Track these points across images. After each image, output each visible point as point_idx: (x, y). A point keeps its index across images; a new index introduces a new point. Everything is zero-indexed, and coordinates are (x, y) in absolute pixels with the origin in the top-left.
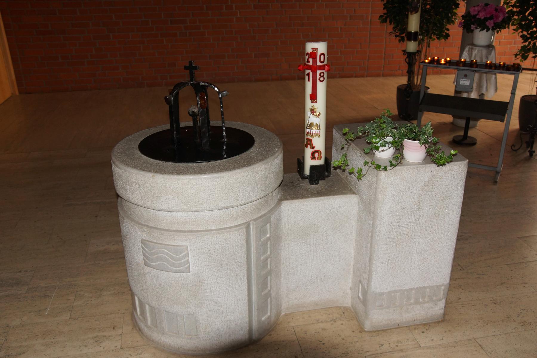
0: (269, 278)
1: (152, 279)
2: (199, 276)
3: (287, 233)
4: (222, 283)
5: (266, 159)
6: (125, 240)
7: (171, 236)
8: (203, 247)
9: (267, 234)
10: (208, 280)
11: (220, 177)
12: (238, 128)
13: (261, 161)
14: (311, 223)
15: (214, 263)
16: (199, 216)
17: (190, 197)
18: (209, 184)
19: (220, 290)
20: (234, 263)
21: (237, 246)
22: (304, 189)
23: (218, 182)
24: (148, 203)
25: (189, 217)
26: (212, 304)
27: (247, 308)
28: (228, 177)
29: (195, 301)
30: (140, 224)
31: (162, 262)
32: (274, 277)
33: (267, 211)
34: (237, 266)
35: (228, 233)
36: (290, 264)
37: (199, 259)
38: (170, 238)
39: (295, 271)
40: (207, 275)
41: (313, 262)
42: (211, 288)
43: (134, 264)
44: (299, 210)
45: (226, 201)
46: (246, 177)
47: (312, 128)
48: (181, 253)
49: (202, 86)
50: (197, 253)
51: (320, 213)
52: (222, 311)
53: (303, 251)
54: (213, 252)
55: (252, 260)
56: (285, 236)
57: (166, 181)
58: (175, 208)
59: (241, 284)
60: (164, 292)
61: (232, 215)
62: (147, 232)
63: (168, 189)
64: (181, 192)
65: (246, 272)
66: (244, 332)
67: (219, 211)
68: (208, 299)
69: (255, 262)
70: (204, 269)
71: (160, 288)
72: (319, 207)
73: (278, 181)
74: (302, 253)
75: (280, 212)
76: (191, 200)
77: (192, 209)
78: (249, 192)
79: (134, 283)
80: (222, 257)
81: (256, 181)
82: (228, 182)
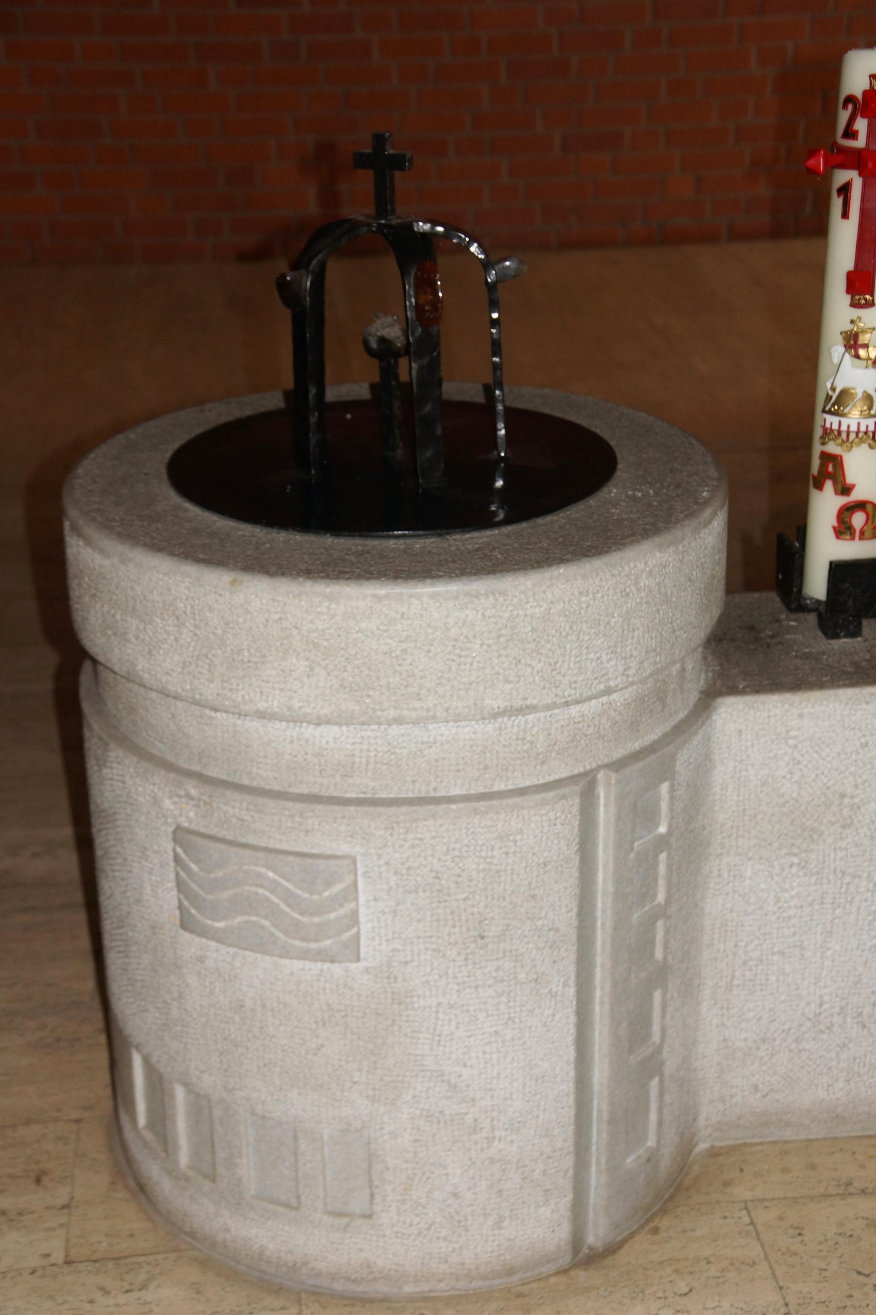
0: (657, 995)
1: (207, 984)
2: (392, 976)
3: (730, 824)
4: (480, 1010)
5: (666, 528)
6: (103, 833)
7: (291, 816)
8: (416, 864)
9: (657, 825)
10: (428, 993)
11: (493, 594)
12: (547, 410)
13: (647, 534)
14: (828, 788)
15: (454, 926)
16: (403, 741)
17: (373, 668)
18: (448, 620)
19: (470, 1037)
20: (530, 931)
21: (545, 865)
22: (799, 654)
23: (486, 614)
24: (211, 685)
25: (365, 747)
26: (437, 1089)
27: (569, 1114)
28: (524, 592)
29: (370, 1076)
30: (170, 767)
31: (254, 918)
32: (676, 995)
33: (660, 734)
34: (543, 945)
35: (512, 811)
36: (736, 946)
37: (395, 911)
38: (289, 824)
39: (756, 975)
40: (424, 976)
41: (829, 945)
42: (439, 1027)
43: (139, 925)
44: (784, 735)
45: (512, 685)
46: (591, 596)
47: (846, 411)
48: (329, 884)
49: (424, 234)
50: (390, 888)
51: (866, 749)
52: (475, 1120)
53: (792, 898)
54: (453, 886)
55: (599, 923)
56: (724, 835)
57: (285, 605)
58: (314, 708)
59: (553, 1015)
60: (254, 1037)
61: (531, 742)
62: (199, 800)
63: (291, 634)
64: (342, 649)
65: (572, 970)
66: (553, 1212)
67: (482, 726)
68: (422, 1071)
69: (609, 931)
70: (412, 951)
71: (237, 1019)
72: (863, 727)
73: (708, 616)
74: (786, 905)
75: (709, 739)
76: (378, 678)
77: (379, 713)
78: (598, 655)
79: (131, 1000)
80: (486, 906)
81: (627, 612)
82: (521, 613)
